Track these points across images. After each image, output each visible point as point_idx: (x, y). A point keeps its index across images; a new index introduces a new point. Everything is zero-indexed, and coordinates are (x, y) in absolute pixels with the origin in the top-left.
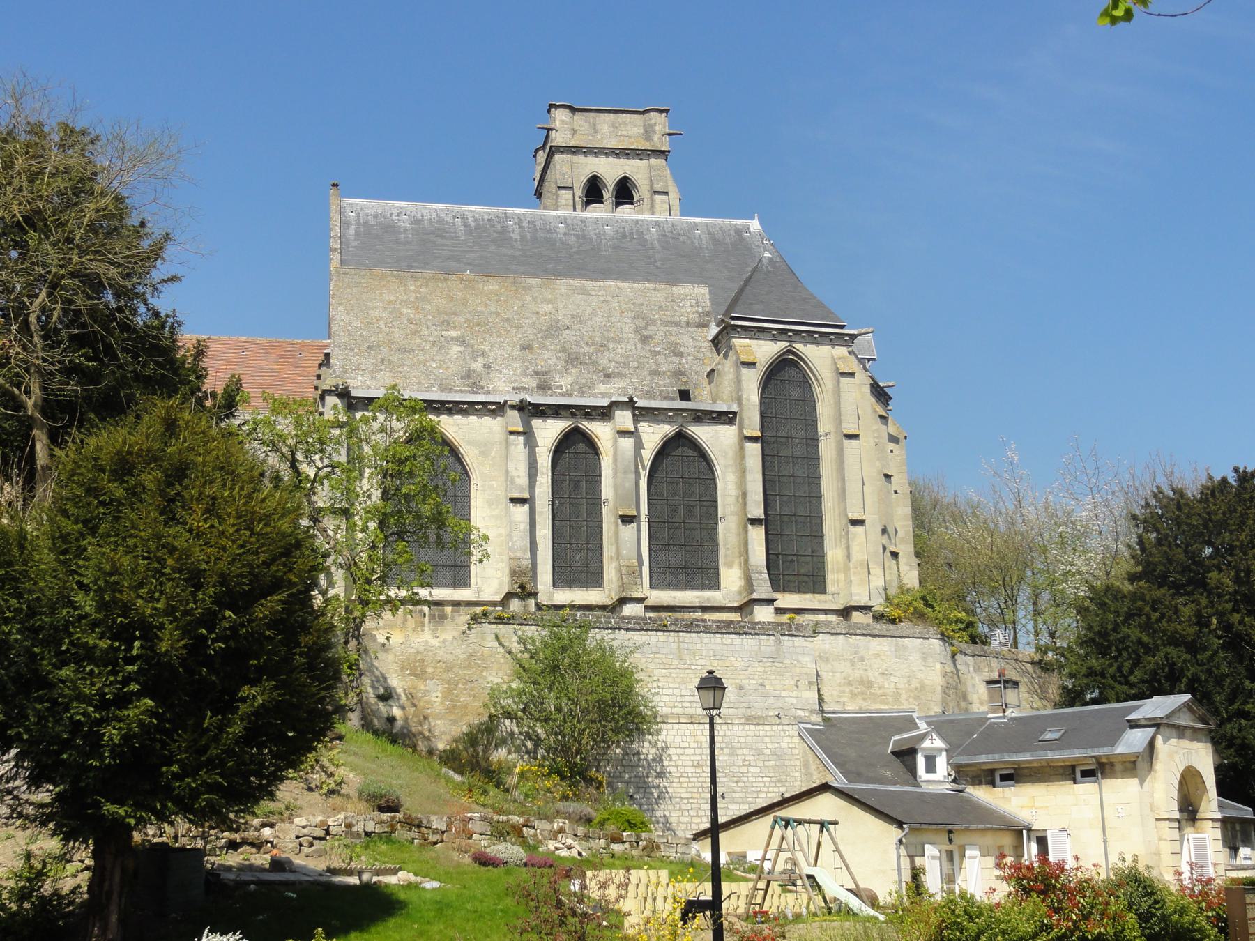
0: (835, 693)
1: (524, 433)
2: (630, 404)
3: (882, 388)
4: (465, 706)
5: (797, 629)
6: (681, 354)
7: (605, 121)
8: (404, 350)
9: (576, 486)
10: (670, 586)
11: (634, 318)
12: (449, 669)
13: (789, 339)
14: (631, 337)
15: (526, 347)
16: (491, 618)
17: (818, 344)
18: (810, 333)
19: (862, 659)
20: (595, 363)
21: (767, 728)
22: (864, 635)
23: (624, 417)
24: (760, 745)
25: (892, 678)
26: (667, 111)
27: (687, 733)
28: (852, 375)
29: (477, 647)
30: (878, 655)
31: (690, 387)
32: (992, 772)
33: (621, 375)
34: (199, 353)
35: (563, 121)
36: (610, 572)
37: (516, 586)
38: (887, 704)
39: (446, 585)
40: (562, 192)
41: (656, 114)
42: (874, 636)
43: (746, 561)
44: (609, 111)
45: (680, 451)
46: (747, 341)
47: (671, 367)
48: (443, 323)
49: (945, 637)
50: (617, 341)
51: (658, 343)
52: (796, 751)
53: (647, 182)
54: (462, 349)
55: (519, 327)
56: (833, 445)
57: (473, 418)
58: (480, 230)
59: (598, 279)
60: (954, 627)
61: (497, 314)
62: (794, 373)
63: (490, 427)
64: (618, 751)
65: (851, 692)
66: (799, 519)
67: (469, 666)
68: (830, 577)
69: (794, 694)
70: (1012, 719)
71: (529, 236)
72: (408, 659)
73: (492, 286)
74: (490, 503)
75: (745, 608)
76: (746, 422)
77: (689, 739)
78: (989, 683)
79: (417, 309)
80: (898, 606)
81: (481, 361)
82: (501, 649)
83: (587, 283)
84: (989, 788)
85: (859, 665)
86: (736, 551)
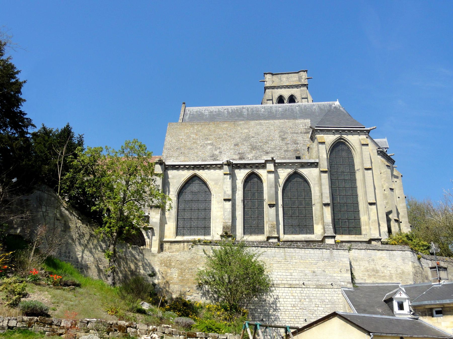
0: (360, 275)
1: (230, 174)
2: (273, 161)
3: (389, 156)
4: (188, 279)
5: (340, 247)
6: (298, 144)
7: (284, 77)
8: (190, 149)
12: (182, 264)
14: (274, 135)
15: (236, 145)
17: (353, 135)
18: (349, 131)
19: (373, 260)
20: (262, 149)
22: (373, 250)
23: (270, 166)
24: (323, 298)
25: (388, 269)
26: (307, 71)
27: (289, 292)
28: (367, 145)
29: (195, 255)
30: (381, 258)
31: (301, 155)
32: (431, 309)
35: (269, 78)
36: (267, 228)
39: (201, 235)
40: (269, 101)
41: (303, 72)
42: (379, 250)
45: (296, 179)
47: (293, 148)
50: (272, 140)
51: (289, 140)
52: (340, 301)
53: (300, 96)
54: (211, 147)
55: (234, 138)
57: (212, 171)
60: (422, 248)
61: (226, 134)
62: (343, 147)
63: (219, 173)
64: (256, 299)
65: (369, 275)
67: (191, 263)
68: (363, 228)
69: (339, 275)
70: (444, 285)
73: (226, 125)
74: (218, 202)
75: (323, 241)
76: (321, 166)
77: (290, 294)
78: (431, 268)
79: (197, 135)
80: (395, 240)
81: (218, 151)
82: (205, 256)
83: (262, 121)
84: (430, 317)
85: (372, 263)
86: (320, 218)
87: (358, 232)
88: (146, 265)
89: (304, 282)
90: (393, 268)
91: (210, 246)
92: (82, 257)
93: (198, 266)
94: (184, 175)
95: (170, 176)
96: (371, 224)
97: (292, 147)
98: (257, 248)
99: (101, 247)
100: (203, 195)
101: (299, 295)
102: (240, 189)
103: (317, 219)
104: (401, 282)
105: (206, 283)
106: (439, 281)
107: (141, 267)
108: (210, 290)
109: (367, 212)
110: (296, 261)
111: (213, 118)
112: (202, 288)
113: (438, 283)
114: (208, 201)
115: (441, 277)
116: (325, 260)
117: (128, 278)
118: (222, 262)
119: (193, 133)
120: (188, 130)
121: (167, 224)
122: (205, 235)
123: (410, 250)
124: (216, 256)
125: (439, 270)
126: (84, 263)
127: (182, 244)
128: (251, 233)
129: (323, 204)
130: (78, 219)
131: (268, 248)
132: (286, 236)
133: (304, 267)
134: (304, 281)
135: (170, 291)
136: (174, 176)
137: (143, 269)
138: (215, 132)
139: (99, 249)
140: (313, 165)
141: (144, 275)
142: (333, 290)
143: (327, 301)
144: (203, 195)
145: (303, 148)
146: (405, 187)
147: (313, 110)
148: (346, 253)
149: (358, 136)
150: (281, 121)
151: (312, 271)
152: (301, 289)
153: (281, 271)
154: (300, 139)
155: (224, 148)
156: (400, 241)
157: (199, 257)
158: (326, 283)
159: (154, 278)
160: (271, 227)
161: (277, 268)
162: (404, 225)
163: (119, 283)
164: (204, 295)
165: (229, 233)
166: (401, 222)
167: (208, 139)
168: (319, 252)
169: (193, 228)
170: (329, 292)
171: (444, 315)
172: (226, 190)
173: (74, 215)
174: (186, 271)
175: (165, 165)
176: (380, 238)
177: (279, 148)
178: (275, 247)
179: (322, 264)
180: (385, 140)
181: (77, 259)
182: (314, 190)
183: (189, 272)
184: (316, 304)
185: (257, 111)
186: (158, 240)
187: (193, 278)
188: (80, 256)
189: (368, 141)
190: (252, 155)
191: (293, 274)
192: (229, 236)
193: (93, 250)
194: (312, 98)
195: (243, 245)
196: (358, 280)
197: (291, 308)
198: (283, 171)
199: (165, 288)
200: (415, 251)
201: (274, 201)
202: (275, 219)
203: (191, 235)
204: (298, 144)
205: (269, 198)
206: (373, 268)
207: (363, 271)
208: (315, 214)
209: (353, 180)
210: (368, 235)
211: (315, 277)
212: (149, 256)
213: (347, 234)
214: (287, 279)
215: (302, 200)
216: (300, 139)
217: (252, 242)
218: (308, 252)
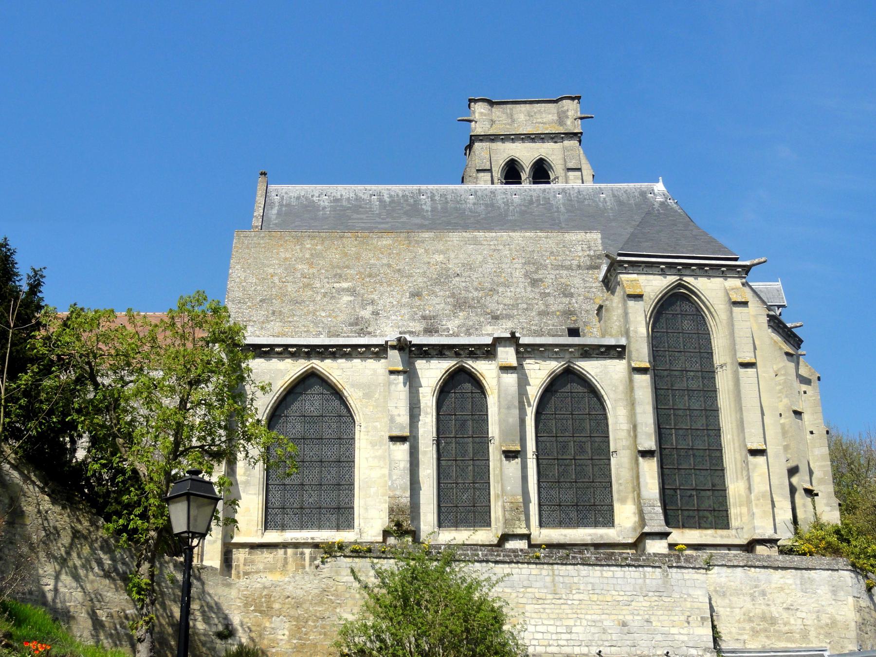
0: (734, 630)
1: (404, 372)
2: (513, 340)
3: (790, 329)
5: (686, 560)
6: (571, 295)
8: (296, 302)
9: (463, 424)
10: (561, 524)
11: (525, 263)
12: (298, 605)
13: (679, 273)
14: (515, 278)
15: (416, 294)
16: (347, 552)
17: (709, 277)
19: (763, 594)
20: (483, 306)
25: (799, 614)
26: (579, 98)
28: (745, 304)
29: (331, 582)
30: (782, 589)
33: (509, 317)
34: (35, 287)
35: (481, 113)
36: (497, 511)
37: (393, 524)
38: (794, 642)
39: (330, 528)
40: (481, 174)
42: (776, 568)
43: (639, 495)
44: (525, 102)
46: (635, 276)
47: (561, 307)
48: (335, 276)
49: (855, 569)
50: (507, 285)
53: (561, 162)
54: (352, 298)
55: (410, 276)
56: (730, 376)
57: (357, 362)
58: (392, 207)
59: (490, 229)
61: (389, 266)
62: (686, 307)
63: (375, 368)
65: (753, 629)
66: (697, 453)
67: (321, 602)
68: (733, 511)
69: (685, 631)
71: (439, 207)
72: (253, 594)
73: (386, 241)
74: (373, 444)
75: (638, 544)
76: (634, 355)
79: (311, 265)
80: (809, 541)
81: (370, 308)
82: (356, 585)
83: (480, 234)
85: (760, 600)
86: (630, 486)
87: (722, 521)
88: (211, 608)
91: (368, 560)
92: (56, 590)
93: (338, 610)
94: (283, 373)
96: (756, 501)
97: (557, 304)
98: (484, 564)
99: (100, 563)
100: (334, 426)
103: (621, 488)
104: (828, 646)
107: (198, 613)
109: (745, 473)
110: (581, 597)
111: (344, 220)
114: (346, 440)
116: (651, 594)
118: (404, 601)
119: (302, 260)
120: (287, 250)
122: (338, 528)
123: (850, 567)
124: (384, 584)
126: (59, 605)
127: (281, 552)
128: (456, 524)
129: (640, 452)
130: (43, 491)
131: (513, 565)
133: (599, 612)
137: (203, 620)
138: (358, 259)
139: (96, 569)
140: (613, 352)
141: (204, 635)
144: (334, 426)
145: (584, 306)
146: (826, 405)
147: (601, 205)
148: (698, 576)
149: (721, 279)
150: (527, 234)
151: (619, 621)
153: (545, 622)
154: (576, 281)
155: (385, 301)
156: (823, 544)
157: (341, 588)
159: (230, 641)
160: (512, 510)
161: (534, 615)
162: (825, 501)
165: (403, 525)
168: (637, 575)
172: (395, 412)
173: (33, 483)
174: (310, 623)
176: (776, 537)
177: (525, 306)
178: (528, 563)
179: (644, 604)
181: (43, 595)
182: (616, 417)
183: (316, 627)
185: (458, 203)
187: (328, 643)
188: (51, 587)
189: (747, 295)
191: (574, 630)
192: (407, 532)
193: (82, 572)
194: (593, 167)
195: (451, 556)
198: (537, 366)
200: (861, 569)
201: (518, 442)
202: (520, 491)
203: (302, 527)
205: (504, 434)
206: (764, 613)
207: (739, 621)
208: (618, 475)
209: (710, 392)
210: (744, 530)
211: (626, 637)
213: (696, 528)
214: (561, 643)
215: (584, 439)
216: (576, 281)
218: (610, 574)
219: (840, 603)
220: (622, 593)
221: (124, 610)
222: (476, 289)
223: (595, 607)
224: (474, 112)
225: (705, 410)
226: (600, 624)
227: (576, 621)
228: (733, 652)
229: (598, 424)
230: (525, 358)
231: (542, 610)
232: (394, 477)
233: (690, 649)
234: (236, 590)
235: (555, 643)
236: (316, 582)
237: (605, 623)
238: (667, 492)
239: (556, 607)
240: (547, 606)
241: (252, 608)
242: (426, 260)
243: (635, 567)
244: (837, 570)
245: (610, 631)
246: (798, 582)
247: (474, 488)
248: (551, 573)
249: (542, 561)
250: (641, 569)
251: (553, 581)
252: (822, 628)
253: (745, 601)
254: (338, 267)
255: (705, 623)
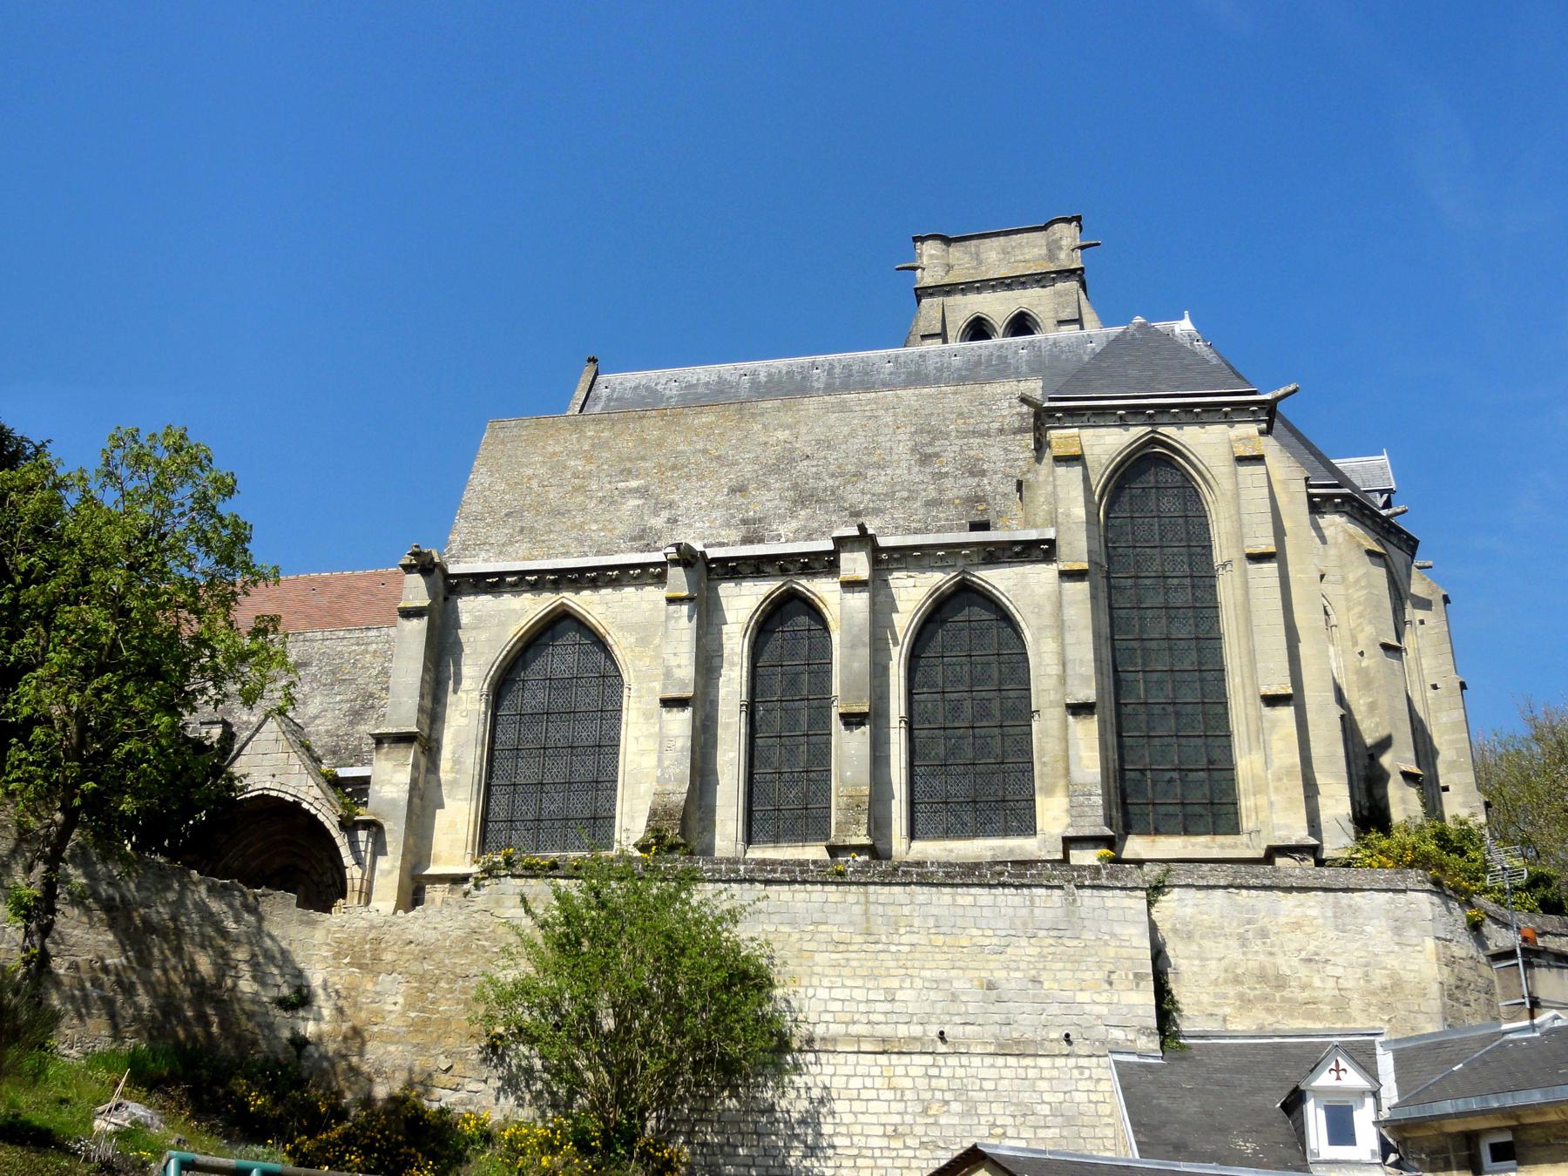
0: (1205, 998)
1: (689, 599)
2: (864, 539)
4: (447, 1021)
6: (983, 473)
8: (557, 513)
9: (793, 681)
13: (1151, 421)
15: (739, 489)
17: (1203, 424)
19: (1263, 934)
21: (1043, 1062)
25: (1329, 969)
26: (1078, 219)
27: (876, 1071)
28: (1259, 459)
29: (487, 918)
30: (1297, 925)
31: (991, 516)
32: (1470, 1139)
35: (931, 256)
38: (1319, 1019)
42: (1289, 889)
47: (963, 492)
48: (621, 472)
52: (1105, 1109)
53: (1052, 314)
54: (641, 502)
56: (1238, 581)
57: (629, 591)
62: (1166, 476)
65: (1241, 997)
67: (467, 950)
68: (1245, 803)
69: (1103, 998)
73: (705, 419)
74: (647, 716)
77: (879, 1082)
79: (589, 459)
81: (665, 514)
85: (1257, 946)
88: (270, 958)
89: (946, 1029)
90: (1351, 965)
94: (517, 614)
95: (465, 619)
97: (957, 489)
98: (747, 886)
101: (922, 1083)
102: (737, 659)
103: (1046, 770)
104: (1386, 1028)
105: (524, 1035)
106: (1532, 1017)
107: (243, 967)
108: (538, 1064)
110: (914, 939)
112: (502, 1058)
113: (1526, 1023)
114: (610, 714)
115: (1541, 994)
116: (1042, 933)
117: (178, 1012)
119: (573, 454)
120: (558, 442)
121: (442, 806)
123: (1428, 886)
125: (1528, 965)
129: (1069, 706)
131: (797, 886)
132: (917, 845)
133: (946, 964)
134: (936, 1020)
135: (365, 1068)
136: (479, 619)
137: (254, 978)
140: (1036, 553)
142: (1072, 1062)
143: (1045, 1110)
145: (1001, 489)
149: (1224, 427)
151: (980, 979)
152: (928, 1059)
153: (848, 983)
158: (1041, 1033)
159: (301, 1013)
161: (829, 971)
162: (1460, 799)
163: (137, 1034)
164: (510, 1084)
166: (1446, 789)
167: (630, 472)
168: (1017, 900)
169: (548, 824)
170: (1055, 1073)
171: (1521, 1163)
172: (673, 662)
174: (443, 984)
175: (447, 576)
177: (905, 494)
178: (824, 883)
179: (1030, 951)
180: (1383, 459)
182: (1039, 654)
183: (451, 991)
184: (994, 1125)
186: (397, 873)
190: (794, 524)
191: (900, 995)
196: (1191, 1021)
197: (884, 1143)
199: (344, 1057)
200: (1455, 890)
204: (983, 473)
206: (1262, 968)
207: (1215, 983)
208: (1041, 750)
209: (1206, 609)
211: (992, 1008)
212: (289, 922)
214: (874, 1018)
215: (991, 695)
217: (728, 860)
219: (1409, 949)
220: (990, 933)
221: (102, 959)
222: (833, 475)
223: (937, 956)
224: (921, 255)
225: (1197, 638)
226: (947, 986)
227: (903, 981)
228: (1202, 1037)
229: (1013, 670)
230: (891, 571)
231: (843, 962)
232: (667, 763)
233: (1112, 1030)
234: (324, 932)
235: (864, 1019)
236: (461, 918)
237: (956, 984)
238: (1130, 775)
239: (869, 956)
240: (853, 955)
241: (347, 960)
242: (763, 439)
243: (1016, 887)
244: (1404, 891)
245: (964, 998)
246: (1330, 914)
247: (809, 780)
248: (862, 899)
249: (848, 879)
250: (1025, 891)
251: (866, 912)
252: (1374, 993)
253: (1227, 947)
254: (630, 460)
255: (1142, 984)
